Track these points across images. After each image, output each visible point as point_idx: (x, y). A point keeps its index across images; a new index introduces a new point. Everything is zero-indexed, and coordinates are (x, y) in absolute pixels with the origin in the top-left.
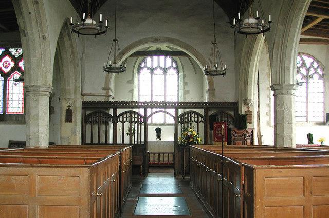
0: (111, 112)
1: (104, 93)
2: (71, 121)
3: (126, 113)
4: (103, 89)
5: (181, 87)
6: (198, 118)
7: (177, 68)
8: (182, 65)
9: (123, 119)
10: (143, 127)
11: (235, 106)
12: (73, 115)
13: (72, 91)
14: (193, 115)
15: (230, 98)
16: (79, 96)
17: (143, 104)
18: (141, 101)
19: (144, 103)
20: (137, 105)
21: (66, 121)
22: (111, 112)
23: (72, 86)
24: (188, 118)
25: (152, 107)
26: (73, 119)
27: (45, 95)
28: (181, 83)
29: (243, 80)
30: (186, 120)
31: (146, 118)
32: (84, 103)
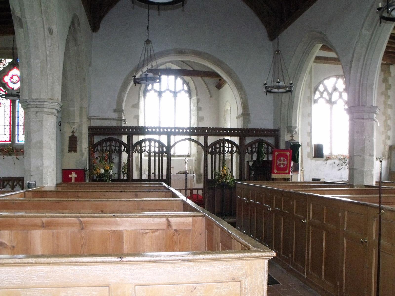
0: (125, 139)
1: (116, 115)
2: (75, 151)
3: (105, 141)
4: (115, 111)
5: (194, 113)
6: (232, 148)
7: (189, 92)
8: (196, 88)
9: (252, 150)
10: (165, 159)
11: (274, 133)
12: (78, 143)
13: (77, 113)
14: (226, 144)
15: (268, 125)
16: (85, 119)
17: (181, 131)
18: (162, 126)
19: (167, 128)
20: (140, 130)
21: (70, 151)
22: (125, 139)
23: (76, 108)
24: (219, 148)
25: (175, 134)
26: (78, 148)
27: (52, 114)
28: (194, 108)
29: (287, 103)
30: (218, 150)
31: (169, 148)
32: (91, 129)
